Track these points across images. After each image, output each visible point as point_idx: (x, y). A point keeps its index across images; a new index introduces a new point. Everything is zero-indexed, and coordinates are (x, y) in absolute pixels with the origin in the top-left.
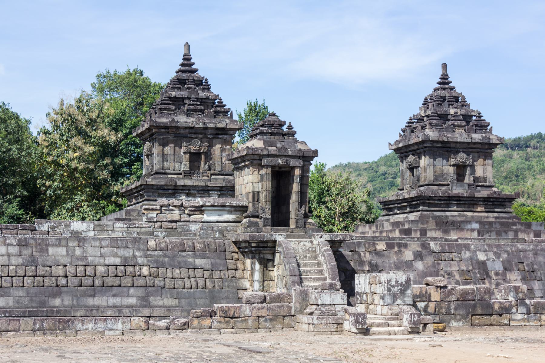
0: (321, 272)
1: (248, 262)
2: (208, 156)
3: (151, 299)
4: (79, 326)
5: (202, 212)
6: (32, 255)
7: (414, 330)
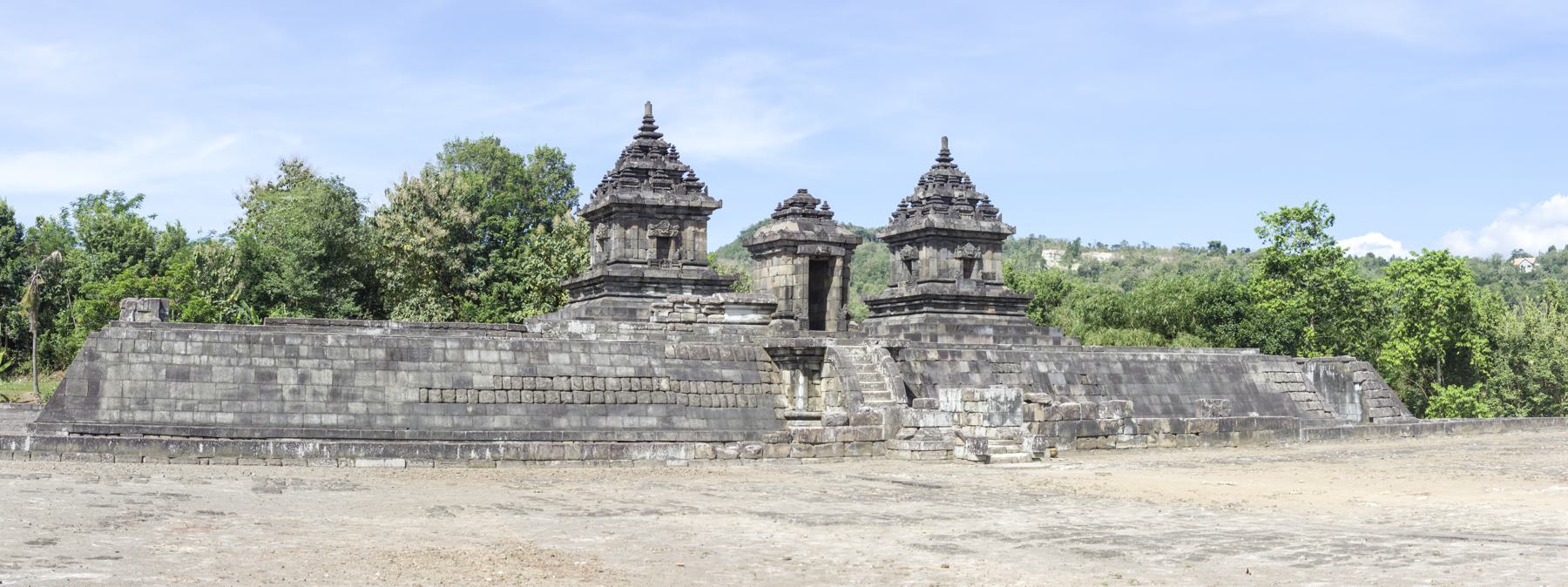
0: (882, 386)
1: (786, 374)
2: (679, 241)
3: (675, 419)
4: (635, 454)
5: (722, 311)
6: (529, 364)
7: (1037, 456)
